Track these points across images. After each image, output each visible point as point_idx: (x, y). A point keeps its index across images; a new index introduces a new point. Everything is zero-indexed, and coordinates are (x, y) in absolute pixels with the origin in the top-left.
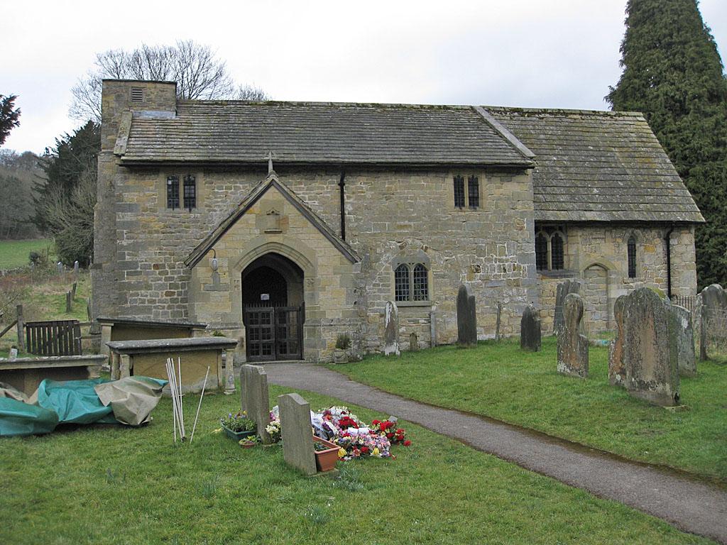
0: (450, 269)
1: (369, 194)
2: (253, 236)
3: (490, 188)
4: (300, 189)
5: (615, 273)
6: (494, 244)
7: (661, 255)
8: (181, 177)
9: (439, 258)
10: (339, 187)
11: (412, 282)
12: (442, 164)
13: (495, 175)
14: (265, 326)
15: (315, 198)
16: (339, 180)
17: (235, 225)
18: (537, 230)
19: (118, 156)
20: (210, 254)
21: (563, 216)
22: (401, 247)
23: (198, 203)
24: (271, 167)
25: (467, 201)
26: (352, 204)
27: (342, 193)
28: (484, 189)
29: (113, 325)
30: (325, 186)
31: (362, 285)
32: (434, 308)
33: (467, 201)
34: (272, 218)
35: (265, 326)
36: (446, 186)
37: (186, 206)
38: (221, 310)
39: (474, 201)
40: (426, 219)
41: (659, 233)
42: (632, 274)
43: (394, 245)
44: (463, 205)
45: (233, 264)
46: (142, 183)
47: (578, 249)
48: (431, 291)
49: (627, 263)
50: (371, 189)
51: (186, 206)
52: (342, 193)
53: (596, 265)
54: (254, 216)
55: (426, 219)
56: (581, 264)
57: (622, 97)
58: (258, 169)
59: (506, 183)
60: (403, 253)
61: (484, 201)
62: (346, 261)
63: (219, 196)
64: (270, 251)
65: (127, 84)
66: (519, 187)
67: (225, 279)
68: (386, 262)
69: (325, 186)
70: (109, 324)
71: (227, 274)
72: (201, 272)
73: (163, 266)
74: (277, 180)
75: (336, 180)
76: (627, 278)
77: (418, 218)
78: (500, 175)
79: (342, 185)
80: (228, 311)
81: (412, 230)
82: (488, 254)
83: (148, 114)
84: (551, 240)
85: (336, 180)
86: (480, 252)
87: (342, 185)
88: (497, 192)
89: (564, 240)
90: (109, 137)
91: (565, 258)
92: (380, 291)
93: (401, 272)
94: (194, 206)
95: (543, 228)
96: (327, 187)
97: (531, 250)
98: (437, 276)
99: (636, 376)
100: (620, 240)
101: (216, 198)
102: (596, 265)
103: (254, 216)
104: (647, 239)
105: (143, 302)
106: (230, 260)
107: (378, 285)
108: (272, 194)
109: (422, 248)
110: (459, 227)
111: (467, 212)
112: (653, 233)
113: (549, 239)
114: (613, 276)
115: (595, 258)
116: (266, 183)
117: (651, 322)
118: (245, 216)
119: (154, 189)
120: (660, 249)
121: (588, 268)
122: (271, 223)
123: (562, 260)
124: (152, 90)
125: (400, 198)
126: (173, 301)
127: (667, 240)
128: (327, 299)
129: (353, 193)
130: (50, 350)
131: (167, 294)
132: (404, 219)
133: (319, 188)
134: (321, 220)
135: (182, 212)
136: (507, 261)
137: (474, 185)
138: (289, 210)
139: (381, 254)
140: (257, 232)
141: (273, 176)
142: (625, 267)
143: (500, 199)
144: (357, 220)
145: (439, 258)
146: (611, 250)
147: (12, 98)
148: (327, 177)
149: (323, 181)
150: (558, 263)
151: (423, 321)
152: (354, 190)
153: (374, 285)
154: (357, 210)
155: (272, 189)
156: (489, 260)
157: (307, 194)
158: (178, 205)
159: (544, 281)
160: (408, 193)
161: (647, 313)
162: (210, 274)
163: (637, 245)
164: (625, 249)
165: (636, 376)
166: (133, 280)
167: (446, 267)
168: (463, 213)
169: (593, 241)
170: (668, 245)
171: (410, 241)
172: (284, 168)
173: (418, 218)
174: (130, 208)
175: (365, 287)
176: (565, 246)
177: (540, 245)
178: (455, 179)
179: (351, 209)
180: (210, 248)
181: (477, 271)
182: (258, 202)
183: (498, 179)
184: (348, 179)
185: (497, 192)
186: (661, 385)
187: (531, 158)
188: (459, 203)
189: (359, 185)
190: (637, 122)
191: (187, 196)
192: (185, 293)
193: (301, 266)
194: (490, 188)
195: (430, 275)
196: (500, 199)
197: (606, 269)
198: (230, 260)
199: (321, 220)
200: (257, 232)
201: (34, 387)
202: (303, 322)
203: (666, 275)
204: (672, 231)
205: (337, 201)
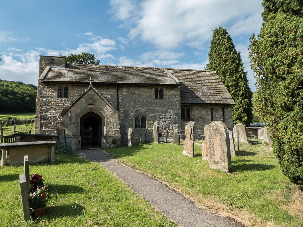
0: (153, 118)
1: (127, 94)
2: (84, 106)
3: (167, 93)
4: (104, 92)
5: (207, 120)
6: (167, 110)
7: (221, 115)
9: (150, 114)
10: (117, 91)
12: (151, 84)
13: (168, 88)
14: (88, 136)
15: (109, 95)
16: (117, 89)
17: (78, 102)
18: (181, 106)
21: (190, 102)
22: (137, 111)
23: (69, 96)
26: (121, 97)
28: (164, 92)
29: (20, 136)
30: (112, 91)
31: (124, 123)
34: (91, 100)
35: (88, 136)
36: (152, 92)
39: (161, 97)
40: (145, 102)
41: (220, 107)
44: (158, 98)
45: (77, 115)
47: (195, 112)
49: (85, 95)
50: (127, 92)
52: (118, 93)
53: (200, 117)
54: (84, 99)
55: (145, 102)
56: (196, 117)
57: (210, 68)
58: (87, 84)
59: (171, 91)
60: (138, 113)
61: (164, 96)
64: (90, 111)
65: (48, 57)
67: (74, 120)
68: (132, 115)
69: (112, 91)
70: (19, 136)
71: (75, 119)
74: (93, 87)
75: (116, 89)
77: (143, 101)
78: (170, 88)
79: (118, 90)
80: (75, 131)
81: (140, 105)
85: (116, 89)
86: (163, 112)
87: (118, 90)
88: (169, 94)
89: (190, 109)
91: (191, 115)
92: (130, 125)
93: (137, 119)
96: (113, 91)
97: (179, 112)
99: (212, 159)
100: (208, 110)
101: (75, 94)
102: (200, 117)
103: (84, 99)
104: (217, 109)
105: (49, 129)
106: (76, 114)
107: (130, 123)
108: (91, 92)
109: (144, 111)
110: (156, 104)
111: (159, 100)
112: (219, 107)
113: (186, 109)
114: (206, 121)
115: (200, 115)
116: (89, 88)
117: (219, 136)
118: (81, 99)
120: (221, 113)
121: (198, 118)
123: (190, 115)
124: (57, 60)
125: (137, 95)
129: (122, 93)
132: (138, 102)
133: (110, 91)
134: (233, 138)
136: (172, 115)
137: (161, 91)
139: (131, 113)
142: (210, 118)
143: (169, 96)
144: (123, 102)
145: (150, 114)
148: (113, 88)
149: (112, 89)
151: (144, 135)
152: (122, 92)
153: (128, 123)
155: (91, 90)
156: (165, 115)
157: (106, 93)
159: (184, 122)
160: (140, 93)
161: (217, 132)
163: (214, 111)
164: (210, 112)
165: (212, 159)
167: (152, 117)
168: (157, 100)
169: (200, 110)
171: (140, 109)
175: (125, 124)
176: (191, 111)
177: (183, 111)
178: (155, 89)
179: (121, 98)
181: (162, 119)
184: (120, 89)
185: (169, 94)
186: (223, 163)
188: (156, 97)
189: (124, 91)
190: (214, 75)
191: (65, 93)
194: (167, 93)
196: (169, 96)
197: (204, 119)
198: (76, 114)
199: (233, 138)
201: (134, 141)
202: (102, 135)
204: (225, 107)
205: (116, 96)
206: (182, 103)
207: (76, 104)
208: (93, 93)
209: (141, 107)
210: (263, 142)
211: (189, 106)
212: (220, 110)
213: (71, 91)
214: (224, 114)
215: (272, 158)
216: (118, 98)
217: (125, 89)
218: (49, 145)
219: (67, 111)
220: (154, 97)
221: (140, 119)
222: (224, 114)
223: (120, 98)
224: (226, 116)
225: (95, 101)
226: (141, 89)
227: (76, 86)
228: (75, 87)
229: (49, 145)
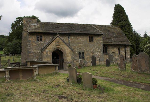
8: (39, 35)
11: (81, 55)
19: (28, 31)
20: (46, 49)
24: (57, 33)
25: (91, 41)
27: (69, 39)
32: (86, 60)
33: (91, 41)
34: (58, 43)
37: (40, 41)
38: (48, 59)
42: (119, 54)
43: (78, 48)
46: (32, 36)
48: (85, 57)
49: (118, 52)
51: (40, 41)
52: (69, 39)
62: (71, 51)
63: (46, 39)
66: (100, 38)
67: (49, 54)
72: (44, 53)
73: (36, 52)
75: (68, 36)
76: (118, 55)
77: (82, 44)
79: (69, 37)
82: (95, 48)
83: (32, 24)
84: (106, 47)
86: (94, 50)
89: (107, 48)
90: (25, 28)
93: (80, 53)
94: (42, 41)
95: (104, 46)
98: (86, 54)
111: (91, 43)
115: (113, 51)
119: (33, 39)
122: (57, 44)
126: (38, 58)
127: (125, 48)
128: (68, 57)
130: (18, 66)
131: (37, 57)
132: (80, 44)
135: (39, 42)
137: (92, 38)
138: (61, 41)
140: (55, 45)
141: (58, 35)
142: (118, 53)
146: (116, 50)
147: (145, 34)
150: (106, 52)
154: (72, 42)
155: (58, 37)
156: (95, 51)
158: (39, 41)
162: (46, 53)
163: (120, 49)
166: (30, 55)
170: (125, 49)
172: (60, 34)
173: (82, 44)
174: (30, 41)
180: (46, 48)
182: (55, 40)
183: (96, 37)
184: (70, 36)
187: (102, 33)
188: (90, 41)
192: (41, 57)
193: (63, 52)
195: (85, 54)
197: (115, 53)
200: (55, 45)
203: (125, 54)
206: (103, 45)
207: (50, 45)
208: (59, 39)
209: (81, 47)
210: (8, 76)
211: (107, 46)
212: (123, 48)
213: (43, 38)
214: (125, 50)
215: (99, 97)
216: (69, 42)
217: (73, 36)
218: (55, 66)
219: (45, 49)
220: (88, 41)
221: (81, 53)
222: (125, 50)
223: (70, 41)
224: (126, 52)
225: (60, 43)
226: (82, 37)
227: (46, 35)
228: (46, 35)
229: (55, 66)
